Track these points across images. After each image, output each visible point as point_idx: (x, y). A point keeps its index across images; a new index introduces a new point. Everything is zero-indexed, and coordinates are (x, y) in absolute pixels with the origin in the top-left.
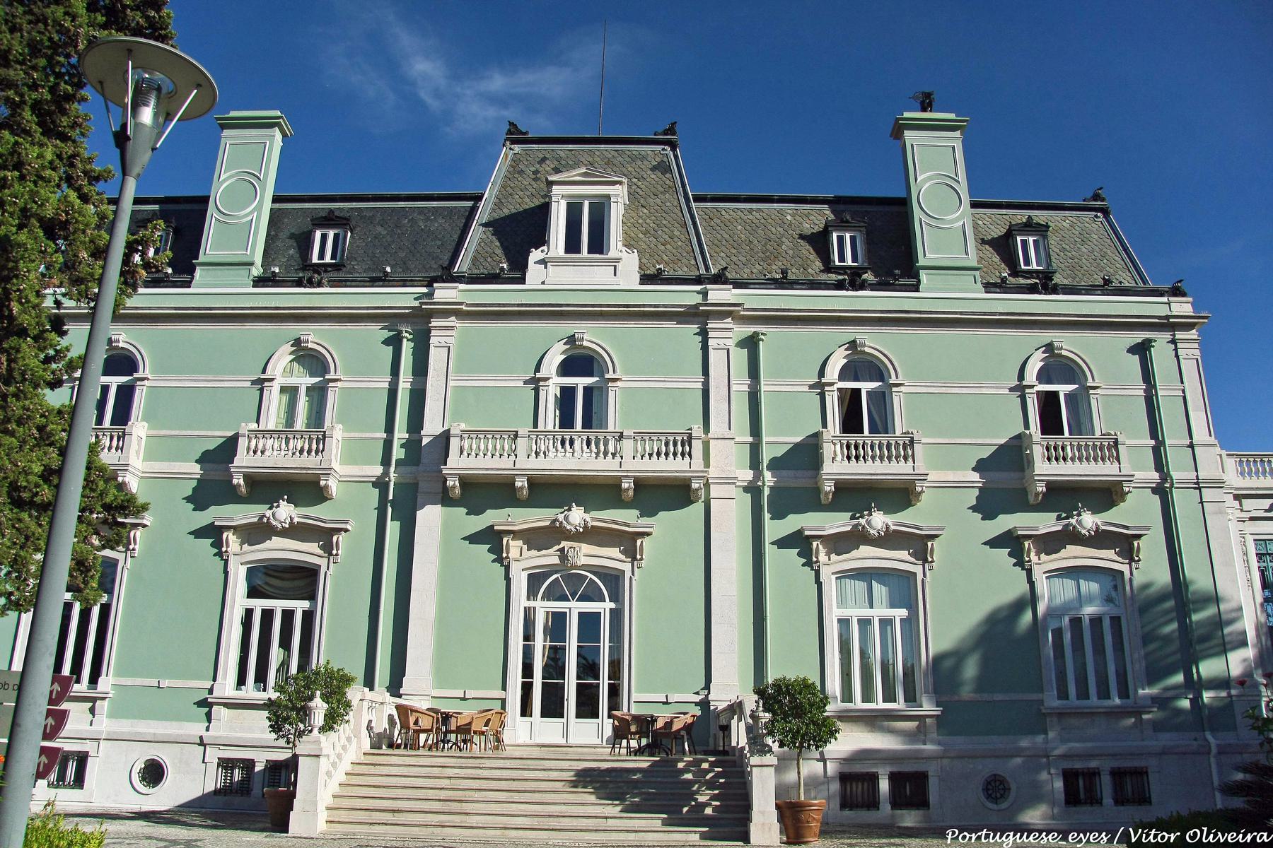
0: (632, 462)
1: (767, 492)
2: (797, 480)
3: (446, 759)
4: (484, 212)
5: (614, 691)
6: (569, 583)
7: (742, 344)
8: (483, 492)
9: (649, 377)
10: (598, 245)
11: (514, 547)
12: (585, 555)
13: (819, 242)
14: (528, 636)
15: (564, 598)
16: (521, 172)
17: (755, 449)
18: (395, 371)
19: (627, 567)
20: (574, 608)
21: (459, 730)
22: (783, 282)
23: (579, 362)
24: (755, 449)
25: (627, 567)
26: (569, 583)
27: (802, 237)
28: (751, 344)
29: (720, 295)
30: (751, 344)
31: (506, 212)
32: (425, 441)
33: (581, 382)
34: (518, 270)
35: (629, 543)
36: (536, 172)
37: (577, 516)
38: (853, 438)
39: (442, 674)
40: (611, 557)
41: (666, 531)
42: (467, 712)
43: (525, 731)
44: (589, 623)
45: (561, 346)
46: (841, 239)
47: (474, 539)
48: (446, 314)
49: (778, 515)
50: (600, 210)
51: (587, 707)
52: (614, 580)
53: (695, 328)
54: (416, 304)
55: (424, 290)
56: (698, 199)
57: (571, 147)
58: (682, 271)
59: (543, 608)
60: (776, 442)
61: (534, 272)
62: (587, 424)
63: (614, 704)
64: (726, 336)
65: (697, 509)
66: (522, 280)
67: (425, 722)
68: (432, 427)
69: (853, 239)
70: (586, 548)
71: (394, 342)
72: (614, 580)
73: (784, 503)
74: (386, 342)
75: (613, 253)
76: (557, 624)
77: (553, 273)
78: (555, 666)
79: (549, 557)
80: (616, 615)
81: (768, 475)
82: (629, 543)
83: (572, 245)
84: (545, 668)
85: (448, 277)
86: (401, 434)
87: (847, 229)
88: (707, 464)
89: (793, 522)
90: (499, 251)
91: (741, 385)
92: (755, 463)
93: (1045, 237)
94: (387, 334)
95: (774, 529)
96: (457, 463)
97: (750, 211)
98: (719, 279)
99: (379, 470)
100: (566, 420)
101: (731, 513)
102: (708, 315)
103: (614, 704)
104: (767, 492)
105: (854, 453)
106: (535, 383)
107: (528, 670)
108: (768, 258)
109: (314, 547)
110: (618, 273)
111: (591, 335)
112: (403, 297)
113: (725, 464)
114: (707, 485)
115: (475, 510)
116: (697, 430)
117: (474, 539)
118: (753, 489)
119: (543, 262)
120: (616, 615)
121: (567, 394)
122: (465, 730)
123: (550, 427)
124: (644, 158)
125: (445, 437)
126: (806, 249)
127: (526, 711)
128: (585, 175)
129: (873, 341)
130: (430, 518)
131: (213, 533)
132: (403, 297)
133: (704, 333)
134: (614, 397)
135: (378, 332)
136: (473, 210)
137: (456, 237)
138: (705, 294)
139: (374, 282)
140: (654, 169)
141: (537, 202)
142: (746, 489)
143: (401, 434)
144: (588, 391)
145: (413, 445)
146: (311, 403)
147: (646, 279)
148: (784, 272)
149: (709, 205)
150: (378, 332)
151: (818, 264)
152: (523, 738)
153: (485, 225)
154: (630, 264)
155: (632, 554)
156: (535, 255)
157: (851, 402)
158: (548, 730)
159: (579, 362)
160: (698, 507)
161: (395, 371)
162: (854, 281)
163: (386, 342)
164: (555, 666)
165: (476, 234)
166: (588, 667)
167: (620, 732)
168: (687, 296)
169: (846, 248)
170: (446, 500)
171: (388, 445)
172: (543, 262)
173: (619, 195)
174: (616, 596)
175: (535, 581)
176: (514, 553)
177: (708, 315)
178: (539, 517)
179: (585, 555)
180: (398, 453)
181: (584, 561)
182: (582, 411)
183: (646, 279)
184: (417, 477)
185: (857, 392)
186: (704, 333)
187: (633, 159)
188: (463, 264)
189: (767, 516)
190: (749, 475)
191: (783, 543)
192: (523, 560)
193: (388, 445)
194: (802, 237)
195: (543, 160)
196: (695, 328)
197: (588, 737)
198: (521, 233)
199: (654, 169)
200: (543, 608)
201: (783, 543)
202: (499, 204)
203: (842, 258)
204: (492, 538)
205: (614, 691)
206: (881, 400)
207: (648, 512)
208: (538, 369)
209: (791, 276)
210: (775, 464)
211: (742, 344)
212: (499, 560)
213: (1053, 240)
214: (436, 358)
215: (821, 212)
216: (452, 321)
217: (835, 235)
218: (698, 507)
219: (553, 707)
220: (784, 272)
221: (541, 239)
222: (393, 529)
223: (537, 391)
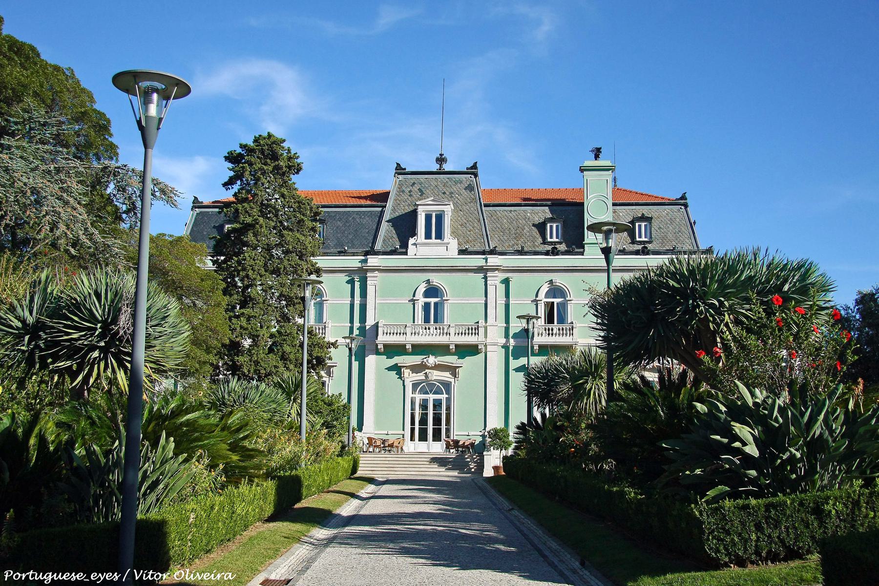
0: (455, 340)
1: (511, 348)
2: (522, 342)
3: (383, 455)
4: (387, 216)
5: (448, 430)
6: (428, 387)
7: (503, 282)
8: (392, 350)
9: (462, 299)
10: (439, 236)
11: (406, 372)
12: (436, 375)
13: (541, 227)
14: (413, 409)
15: (427, 393)
16: (403, 191)
17: (507, 329)
18: (353, 296)
19: (452, 380)
20: (431, 397)
21: (389, 446)
22: (521, 252)
23: (432, 291)
24: (507, 329)
25: (452, 380)
26: (428, 387)
27: (534, 225)
28: (506, 282)
29: (493, 260)
30: (506, 282)
31: (397, 214)
32: (367, 328)
33: (433, 300)
34: (403, 249)
35: (453, 370)
36: (410, 191)
37: (432, 360)
38: (550, 326)
39: (378, 424)
40: (446, 376)
41: (468, 364)
42: (391, 439)
43: (412, 447)
44: (437, 405)
45: (424, 285)
46: (551, 227)
47: (389, 369)
48: (373, 270)
49: (516, 357)
50: (440, 217)
51: (437, 437)
52: (447, 386)
53: (482, 275)
54: (359, 265)
55: (363, 258)
56: (486, 206)
57: (426, 176)
58: (477, 248)
59: (419, 397)
60: (517, 326)
61: (411, 249)
62: (436, 321)
63: (448, 436)
64: (496, 279)
65: (481, 356)
66: (406, 253)
67: (378, 443)
68: (370, 322)
69: (557, 227)
70: (436, 372)
71: (351, 282)
72: (447, 386)
73: (521, 351)
74: (348, 282)
75: (446, 240)
76: (424, 406)
77: (421, 249)
78: (424, 421)
79: (420, 376)
80: (448, 400)
81: (512, 342)
82: (453, 370)
83: (428, 236)
84: (420, 422)
85: (372, 252)
86: (357, 324)
87: (554, 222)
88: (486, 337)
89: (523, 361)
90: (395, 236)
91: (502, 301)
92: (507, 336)
93: (650, 223)
94: (348, 278)
95: (514, 364)
96: (382, 339)
97: (511, 211)
98: (493, 252)
99: (504, 341)
100: (427, 320)
101: (496, 358)
102: (488, 270)
103: (448, 436)
104: (511, 348)
105: (550, 333)
106: (413, 301)
107: (413, 423)
108: (518, 237)
109: (447, 374)
110: (446, 250)
111: (437, 279)
112: (353, 262)
113: (494, 337)
114: (486, 346)
115: (390, 357)
116: (482, 323)
117: (389, 369)
118: (506, 347)
119: (414, 244)
120: (448, 400)
121: (427, 306)
122: (391, 446)
123: (420, 323)
124: (461, 182)
125: (376, 326)
126: (535, 232)
127: (412, 439)
128: (433, 200)
129: (560, 280)
130: (371, 360)
131: (397, 369)
132: (353, 262)
133: (485, 278)
134: (447, 307)
135: (344, 278)
136: (382, 212)
137: (374, 227)
138: (486, 259)
139: (340, 253)
140: (466, 189)
141: (411, 208)
142: (503, 347)
143: (357, 324)
144: (436, 304)
145: (362, 329)
146: (316, 309)
147: (462, 252)
148: (523, 248)
149: (491, 208)
150: (344, 278)
151: (540, 240)
152: (412, 450)
153: (388, 221)
154: (454, 245)
155: (454, 375)
156: (412, 241)
157: (550, 307)
158: (422, 446)
159: (432, 291)
160: (482, 355)
161: (353, 296)
162: (555, 252)
163: (348, 282)
164: (424, 421)
165: (385, 227)
166: (437, 420)
167: (448, 446)
168: (477, 261)
169: (554, 232)
170: (377, 352)
171: (351, 329)
172: (414, 244)
173: (448, 210)
174: (448, 392)
175: (415, 386)
176: (406, 375)
177: (488, 270)
178: (416, 360)
179: (436, 375)
180: (356, 332)
181: (435, 378)
182: (433, 315)
183: (462, 252)
184: (365, 342)
185: (553, 303)
186: (485, 278)
187: (456, 183)
188: (378, 246)
189: (511, 358)
190: (504, 341)
191: (517, 370)
192: (410, 377)
193: (351, 329)
194: (534, 225)
195: (414, 184)
196: (482, 275)
197: (438, 448)
198: (405, 226)
199: (466, 189)
200: (419, 397)
201: (517, 370)
202: (394, 210)
203: (551, 237)
204: (397, 369)
205: (448, 430)
206: (563, 307)
207: (462, 357)
208: (414, 296)
209: (526, 249)
210: (515, 336)
211: (503, 282)
212: (400, 378)
213: (655, 223)
214: (370, 290)
215: (544, 212)
216: (376, 273)
217: (548, 225)
218: (482, 355)
219: (423, 437)
220: (523, 248)
221: (414, 234)
222: (355, 365)
223: (414, 305)
